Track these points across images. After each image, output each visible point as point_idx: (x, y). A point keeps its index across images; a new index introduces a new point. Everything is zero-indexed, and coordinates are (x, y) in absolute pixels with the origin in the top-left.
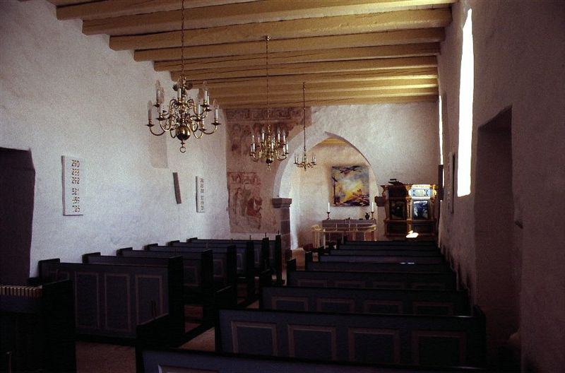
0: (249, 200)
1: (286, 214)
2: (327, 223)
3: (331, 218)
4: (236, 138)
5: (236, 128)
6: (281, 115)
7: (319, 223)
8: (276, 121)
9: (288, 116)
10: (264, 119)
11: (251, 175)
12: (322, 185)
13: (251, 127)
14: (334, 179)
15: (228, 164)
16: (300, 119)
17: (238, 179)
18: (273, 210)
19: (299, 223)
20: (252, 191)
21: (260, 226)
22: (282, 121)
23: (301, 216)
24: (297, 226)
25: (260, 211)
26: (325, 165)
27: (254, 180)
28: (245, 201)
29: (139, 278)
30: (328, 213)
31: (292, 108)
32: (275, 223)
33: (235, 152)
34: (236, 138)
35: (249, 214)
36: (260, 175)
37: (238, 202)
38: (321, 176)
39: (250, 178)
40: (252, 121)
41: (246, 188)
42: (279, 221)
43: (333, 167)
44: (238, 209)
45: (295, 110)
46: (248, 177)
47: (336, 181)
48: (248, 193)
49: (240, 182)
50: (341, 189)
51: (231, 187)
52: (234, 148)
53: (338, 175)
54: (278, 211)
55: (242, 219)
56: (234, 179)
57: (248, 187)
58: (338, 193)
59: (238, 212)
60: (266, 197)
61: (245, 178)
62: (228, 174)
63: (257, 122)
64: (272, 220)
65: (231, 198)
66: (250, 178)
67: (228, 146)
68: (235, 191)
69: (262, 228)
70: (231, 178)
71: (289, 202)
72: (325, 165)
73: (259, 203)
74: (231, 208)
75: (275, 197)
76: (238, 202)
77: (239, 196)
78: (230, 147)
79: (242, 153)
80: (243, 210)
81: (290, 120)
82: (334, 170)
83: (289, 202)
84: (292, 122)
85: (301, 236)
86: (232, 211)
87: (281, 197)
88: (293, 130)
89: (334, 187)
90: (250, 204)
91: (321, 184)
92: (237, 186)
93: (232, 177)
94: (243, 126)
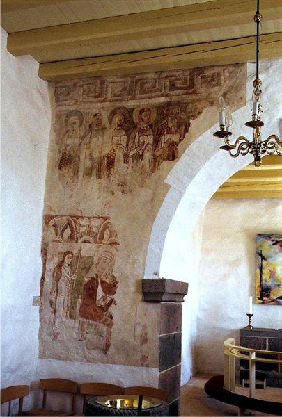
0: (86, 279)
1: (173, 317)
2: (248, 337)
3: (255, 324)
4: (69, 142)
5: (74, 119)
6: (173, 86)
7: (231, 334)
8: (163, 100)
9: (191, 86)
10: (134, 98)
11: (96, 223)
12: (237, 265)
13: (105, 115)
14: (260, 255)
15: (49, 192)
16: (217, 92)
17: (68, 231)
18: (142, 307)
19: (195, 336)
20: (96, 259)
21: (107, 346)
22: (175, 99)
23: (198, 318)
24: (192, 337)
25: (112, 309)
26: (246, 231)
27: (104, 234)
28: (79, 283)
29: (247, 385)
30: (250, 316)
31: (200, 70)
32: (144, 340)
33: (65, 171)
34: (69, 142)
35: (84, 314)
36: (118, 224)
37: (63, 285)
38: (240, 251)
39: (95, 230)
40: (107, 104)
41: (83, 253)
42: (155, 335)
43: (260, 235)
44: (62, 301)
45: (208, 73)
46: (89, 227)
47: (263, 258)
48: (87, 265)
49: (72, 238)
50: (272, 274)
51: (51, 250)
52: (65, 161)
53: (267, 246)
54: (154, 311)
55: (69, 327)
56: (59, 231)
57: (88, 250)
58: (269, 282)
59: (60, 310)
60: (128, 273)
61: (83, 229)
62: (47, 219)
63: (118, 104)
64: (139, 331)
65: (48, 274)
66: (95, 230)
67: (51, 160)
68: (57, 260)
69: (112, 350)
70: (52, 230)
71: (180, 290)
72: (246, 231)
73: (110, 288)
74: (46, 300)
75: (149, 276)
76: (63, 285)
77: (66, 271)
78: (57, 162)
79: (81, 173)
80: (72, 306)
81: (194, 97)
82: (261, 239)
83: (180, 290)
84: (199, 100)
85: (197, 353)
86: (48, 308)
87: (162, 275)
88: (201, 117)
89: (261, 268)
90: (90, 290)
91: (235, 263)
92: (63, 247)
93: (55, 225)
94: (87, 114)
